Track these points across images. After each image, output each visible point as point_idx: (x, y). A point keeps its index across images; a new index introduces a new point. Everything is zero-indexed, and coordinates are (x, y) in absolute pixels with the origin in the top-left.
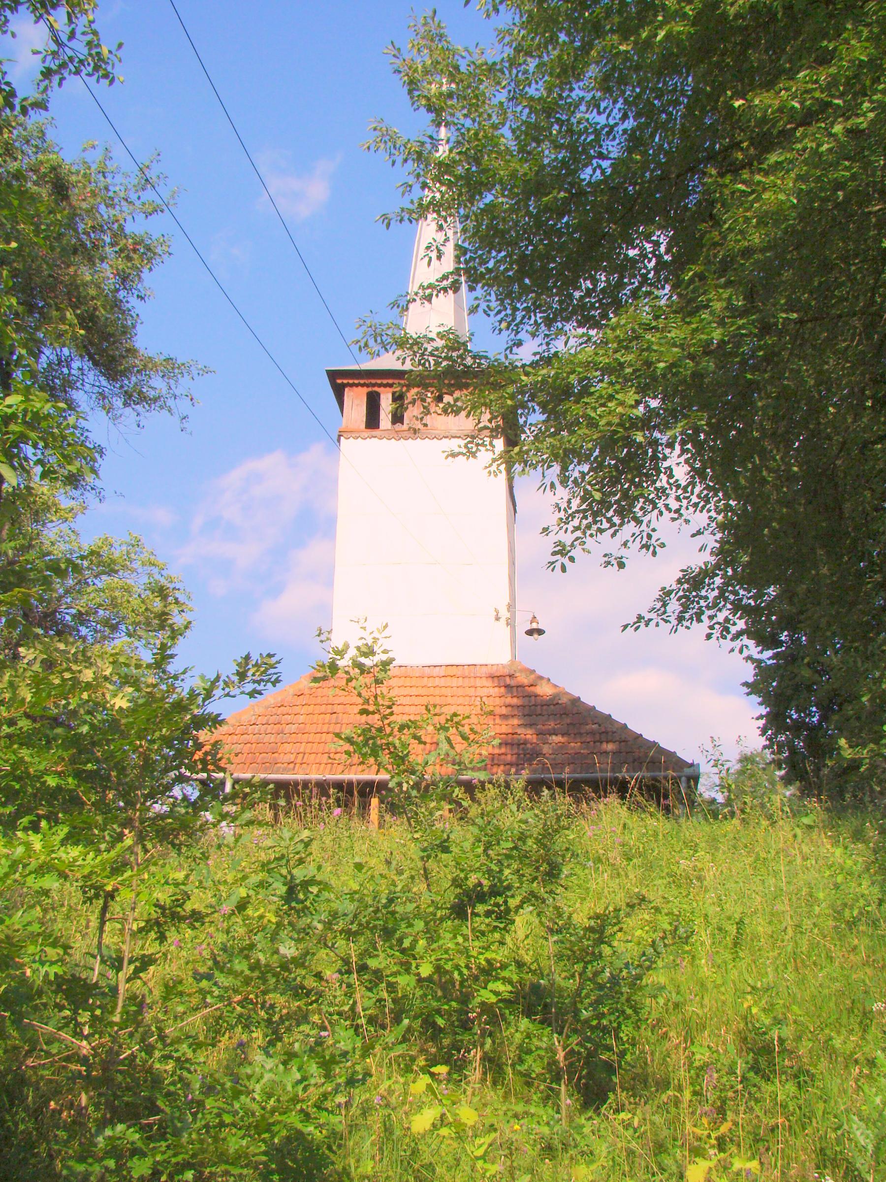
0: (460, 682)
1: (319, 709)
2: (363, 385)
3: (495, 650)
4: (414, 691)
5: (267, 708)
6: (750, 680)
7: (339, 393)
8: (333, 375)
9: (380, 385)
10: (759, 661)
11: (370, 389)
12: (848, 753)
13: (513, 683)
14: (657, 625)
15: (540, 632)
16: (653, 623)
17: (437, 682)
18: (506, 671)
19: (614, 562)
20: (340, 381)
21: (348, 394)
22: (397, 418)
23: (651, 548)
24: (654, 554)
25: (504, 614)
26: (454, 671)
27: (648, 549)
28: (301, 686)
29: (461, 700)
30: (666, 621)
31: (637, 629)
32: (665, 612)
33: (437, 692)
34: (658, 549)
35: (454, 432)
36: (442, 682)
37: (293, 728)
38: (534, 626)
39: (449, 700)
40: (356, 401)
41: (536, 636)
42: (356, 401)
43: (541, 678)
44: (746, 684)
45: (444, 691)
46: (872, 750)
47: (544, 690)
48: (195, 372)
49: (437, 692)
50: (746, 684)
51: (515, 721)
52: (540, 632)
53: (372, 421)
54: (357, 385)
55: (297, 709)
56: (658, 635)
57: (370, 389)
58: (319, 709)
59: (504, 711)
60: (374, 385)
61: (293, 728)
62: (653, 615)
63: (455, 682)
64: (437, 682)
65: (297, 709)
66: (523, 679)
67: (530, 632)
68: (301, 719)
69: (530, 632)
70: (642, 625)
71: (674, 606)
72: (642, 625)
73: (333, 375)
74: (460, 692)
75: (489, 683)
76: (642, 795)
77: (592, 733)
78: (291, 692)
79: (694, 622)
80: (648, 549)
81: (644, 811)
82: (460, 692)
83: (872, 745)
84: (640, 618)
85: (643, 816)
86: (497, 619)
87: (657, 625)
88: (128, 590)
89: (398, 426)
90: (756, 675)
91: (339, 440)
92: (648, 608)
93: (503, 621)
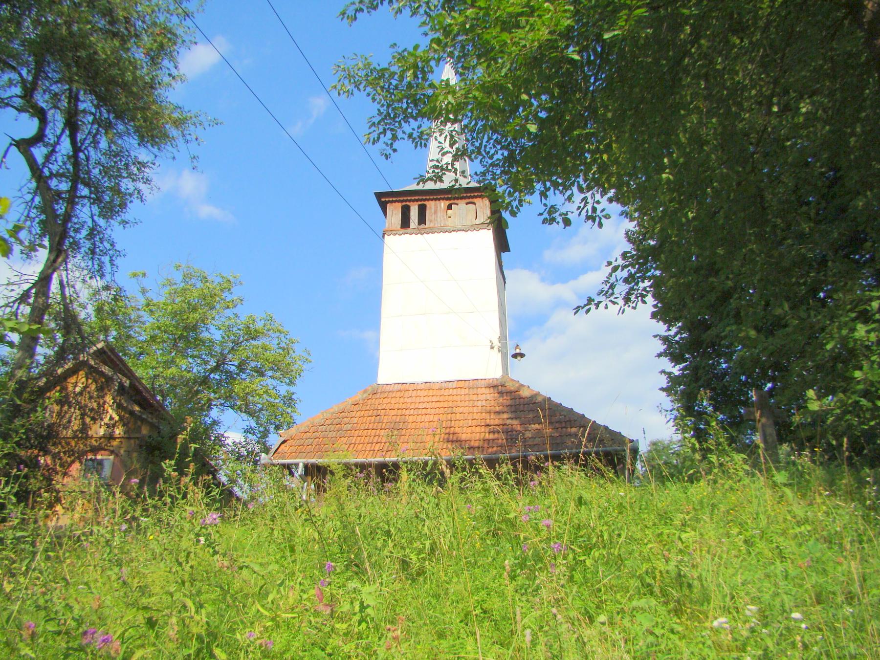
0: (467, 391)
1: (367, 414)
2: (398, 201)
3: (494, 372)
4: (434, 399)
5: (332, 414)
6: (665, 386)
7: (384, 207)
8: (379, 196)
9: (410, 201)
10: (670, 373)
11: (404, 204)
12: (814, 406)
13: (504, 389)
14: (606, 307)
15: (522, 355)
16: (602, 306)
17: (451, 391)
18: (499, 383)
19: (559, 219)
20: (384, 199)
21: (390, 207)
22: (422, 219)
23: (597, 219)
24: (600, 225)
25: (497, 344)
26: (462, 384)
27: (594, 221)
28: (357, 398)
29: (467, 404)
30: (614, 303)
31: (588, 311)
32: (612, 294)
33: (450, 398)
34: (603, 220)
35: (459, 227)
36: (455, 392)
37: (349, 426)
38: (518, 351)
39: (459, 404)
40: (395, 212)
41: (519, 358)
42: (395, 212)
43: (522, 385)
44: (662, 389)
45: (455, 398)
46: (841, 401)
47: (525, 393)
48: (206, 125)
49: (450, 398)
50: (662, 389)
51: (505, 416)
52: (522, 355)
53: (405, 223)
54: (395, 202)
55: (353, 414)
56: (608, 313)
57: (404, 204)
58: (367, 414)
59: (497, 409)
60: (406, 201)
61: (349, 426)
62: (601, 298)
63: (463, 391)
64: (451, 391)
65: (353, 414)
66: (511, 386)
67: (515, 356)
68: (355, 420)
69: (515, 356)
70: (593, 307)
71: (622, 289)
72: (593, 307)
73: (379, 196)
74: (467, 398)
75: (487, 391)
76: (600, 461)
77: (559, 422)
78: (350, 402)
79: (640, 303)
80: (594, 221)
81: (603, 476)
82: (467, 398)
83: (841, 395)
84: (590, 300)
85: (602, 482)
86: (492, 348)
87: (606, 307)
88: (265, 349)
89: (422, 226)
90: (668, 383)
91: (384, 237)
92: (597, 291)
93: (496, 349)
